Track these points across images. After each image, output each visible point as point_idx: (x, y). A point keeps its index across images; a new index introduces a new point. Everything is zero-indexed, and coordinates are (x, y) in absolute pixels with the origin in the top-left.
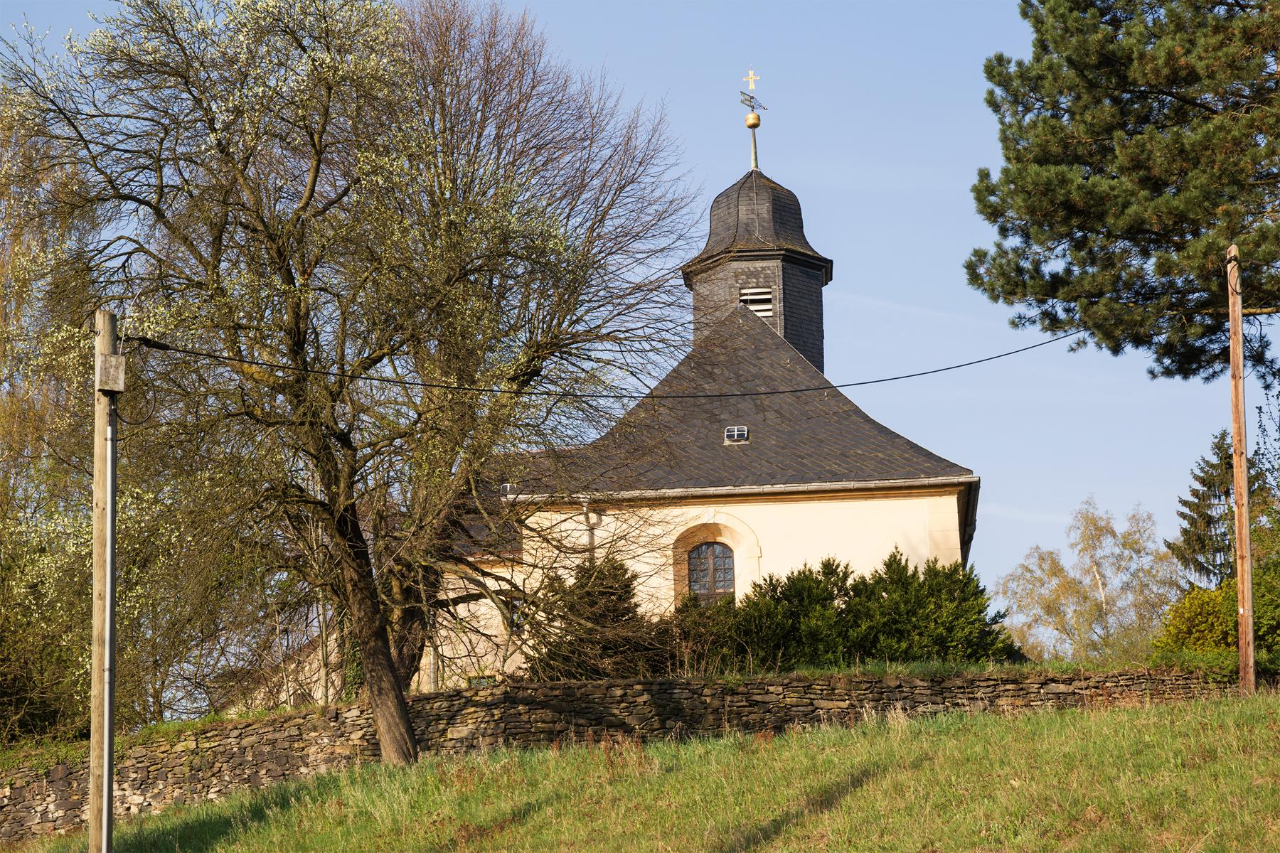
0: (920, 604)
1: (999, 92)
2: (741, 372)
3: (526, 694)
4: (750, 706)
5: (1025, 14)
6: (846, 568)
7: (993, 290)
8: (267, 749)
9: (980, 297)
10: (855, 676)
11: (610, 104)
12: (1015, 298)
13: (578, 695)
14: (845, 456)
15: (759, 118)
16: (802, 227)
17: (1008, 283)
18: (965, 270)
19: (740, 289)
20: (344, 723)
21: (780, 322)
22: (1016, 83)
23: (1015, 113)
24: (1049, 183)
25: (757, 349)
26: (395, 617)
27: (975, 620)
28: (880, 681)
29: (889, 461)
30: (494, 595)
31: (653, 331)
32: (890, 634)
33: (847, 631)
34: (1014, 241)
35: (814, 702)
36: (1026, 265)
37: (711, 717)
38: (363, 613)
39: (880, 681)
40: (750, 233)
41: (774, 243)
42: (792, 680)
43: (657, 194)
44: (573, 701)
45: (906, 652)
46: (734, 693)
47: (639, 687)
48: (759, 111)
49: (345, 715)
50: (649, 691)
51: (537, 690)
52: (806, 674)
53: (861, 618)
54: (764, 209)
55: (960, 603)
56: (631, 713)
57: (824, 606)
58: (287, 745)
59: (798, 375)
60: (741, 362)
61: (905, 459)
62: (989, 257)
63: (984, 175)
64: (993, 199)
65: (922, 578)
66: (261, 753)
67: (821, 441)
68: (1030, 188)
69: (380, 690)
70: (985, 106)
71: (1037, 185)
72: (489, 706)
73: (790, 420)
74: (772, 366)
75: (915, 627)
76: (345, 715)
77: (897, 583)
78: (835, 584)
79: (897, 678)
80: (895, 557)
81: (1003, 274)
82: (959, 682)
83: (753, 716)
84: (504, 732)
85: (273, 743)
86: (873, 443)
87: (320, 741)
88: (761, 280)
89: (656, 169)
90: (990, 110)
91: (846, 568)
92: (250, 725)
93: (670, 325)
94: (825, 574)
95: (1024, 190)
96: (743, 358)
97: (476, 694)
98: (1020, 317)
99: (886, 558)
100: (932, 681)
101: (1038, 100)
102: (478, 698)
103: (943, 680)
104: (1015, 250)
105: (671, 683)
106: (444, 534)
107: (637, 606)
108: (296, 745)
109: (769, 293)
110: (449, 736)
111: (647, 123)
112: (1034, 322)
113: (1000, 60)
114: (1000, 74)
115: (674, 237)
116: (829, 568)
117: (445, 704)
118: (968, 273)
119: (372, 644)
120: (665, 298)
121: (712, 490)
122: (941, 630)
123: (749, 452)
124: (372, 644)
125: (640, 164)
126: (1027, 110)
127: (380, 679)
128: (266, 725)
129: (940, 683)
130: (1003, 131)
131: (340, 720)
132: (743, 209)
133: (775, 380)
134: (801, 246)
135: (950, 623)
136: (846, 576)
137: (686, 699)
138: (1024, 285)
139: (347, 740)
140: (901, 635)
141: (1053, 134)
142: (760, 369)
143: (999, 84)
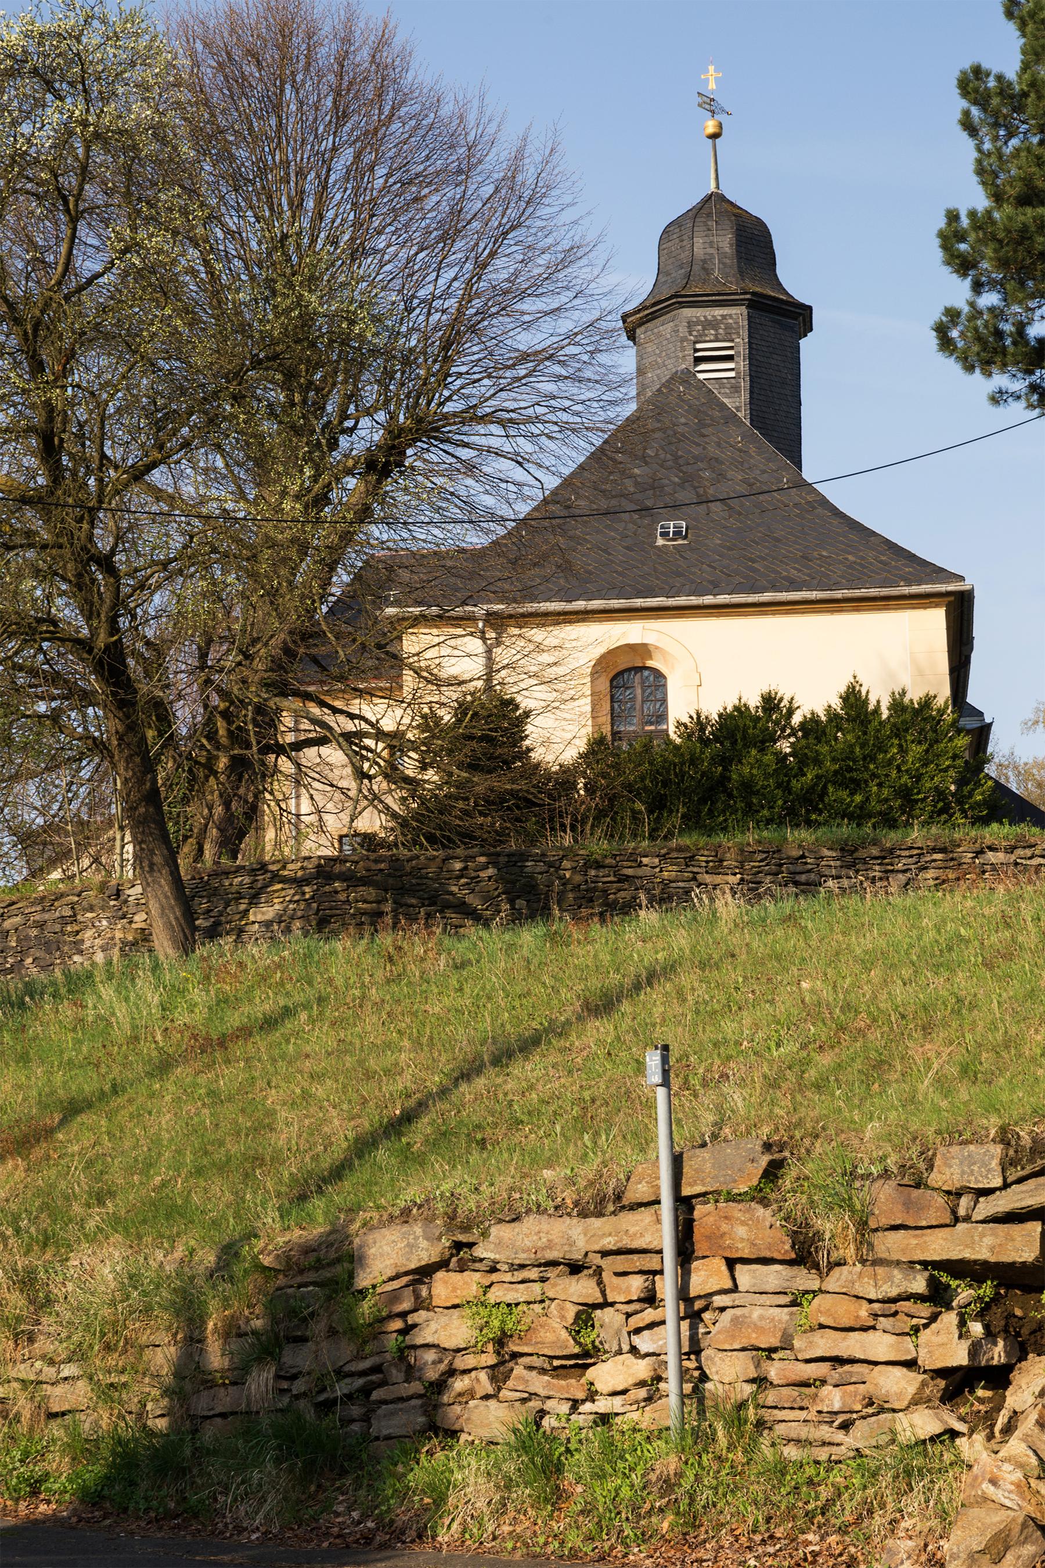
0: (882, 748)
1: (975, 111)
2: (680, 453)
3: (344, 869)
4: (619, 881)
5: (1009, 14)
6: (791, 702)
7: (966, 358)
8: (34, 932)
9: (951, 366)
10: (749, 844)
11: (491, 129)
12: (995, 369)
13: (408, 869)
14: (806, 558)
15: (720, 126)
16: (775, 264)
17: (984, 350)
18: (934, 334)
19: (695, 343)
20: (126, 901)
21: (744, 385)
22: (995, 101)
23: (995, 138)
24: (1024, 229)
25: (702, 424)
26: (221, 765)
27: (949, 767)
28: (779, 851)
29: (860, 565)
30: (341, 740)
31: (546, 410)
32: (842, 785)
33: (789, 781)
34: (990, 299)
35: (699, 877)
36: (1007, 327)
37: (571, 895)
38: (131, 773)
39: (779, 851)
40: (707, 271)
41: (737, 284)
42: (671, 850)
43: (550, 240)
44: (401, 876)
45: (861, 806)
46: (599, 865)
47: (482, 859)
48: (721, 117)
49: (128, 892)
50: (495, 864)
51: (357, 862)
52: (688, 842)
53: (808, 765)
54: (726, 241)
55: (931, 746)
56: (473, 891)
57: (762, 750)
58: (57, 928)
59: (752, 457)
60: (680, 441)
61: (881, 562)
62: (963, 317)
63: (953, 217)
64: (963, 247)
65: (885, 714)
66: (27, 938)
67: (778, 540)
68: (1001, 235)
69: (152, 865)
70: (958, 128)
71: (1010, 232)
72: (298, 882)
73: (740, 514)
74: (719, 444)
75: (874, 776)
76: (128, 892)
77: (854, 720)
78: (777, 723)
79: (800, 846)
80: (854, 688)
81: (979, 338)
82: (875, 851)
83: (622, 894)
84: (316, 914)
85: (41, 925)
86: (843, 543)
87: (97, 924)
88: (721, 331)
89: (548, 210)
90: (965, 135)
91: (791, 702)
92: (13, 903)
93: (567, 403)
94: (764, 709)
95: (994, 238)
96: (683, 435)
97: (284, 868)
98: (1000, 392)
99: (843, 689)
100: (842, 850)
101: (1023, 122)
102: (286, 873)
103: (856, 849)
104: (991, 310)
105: (522, 854)
106: (277, 666)
107: (529, 750)
108: (69, 928)
109: (731, 348)
110: (252, 918)
111: (535, 154)
112: (1019, 397)
113: (978, 72)
114: (976, 90)
115: (572, 295)
116: (770, 702)
117: (247, 880)
118: (938, 337)
119: (142, 810)
120: (558, 369)
121: (639, 602)
122: (905, 779)
123: (688, 554)
124: (142, 810)
125: (528, 203)
126: (1011, 135)
127: (152, 852)
128: (33, 904)
129: (853, 852)
130: (979, 162)
131: (122, 898)
132: (699, 242)
133: (722, 463)
134: (773, 289)
135: (917, 770)
136: (791, 712)
137: (541, 873)
138: (1004, 351)
139: (131, 922)
140: (855, 786)
141: (1039, 165)
142: (704, 448)
143: (975, 103)
